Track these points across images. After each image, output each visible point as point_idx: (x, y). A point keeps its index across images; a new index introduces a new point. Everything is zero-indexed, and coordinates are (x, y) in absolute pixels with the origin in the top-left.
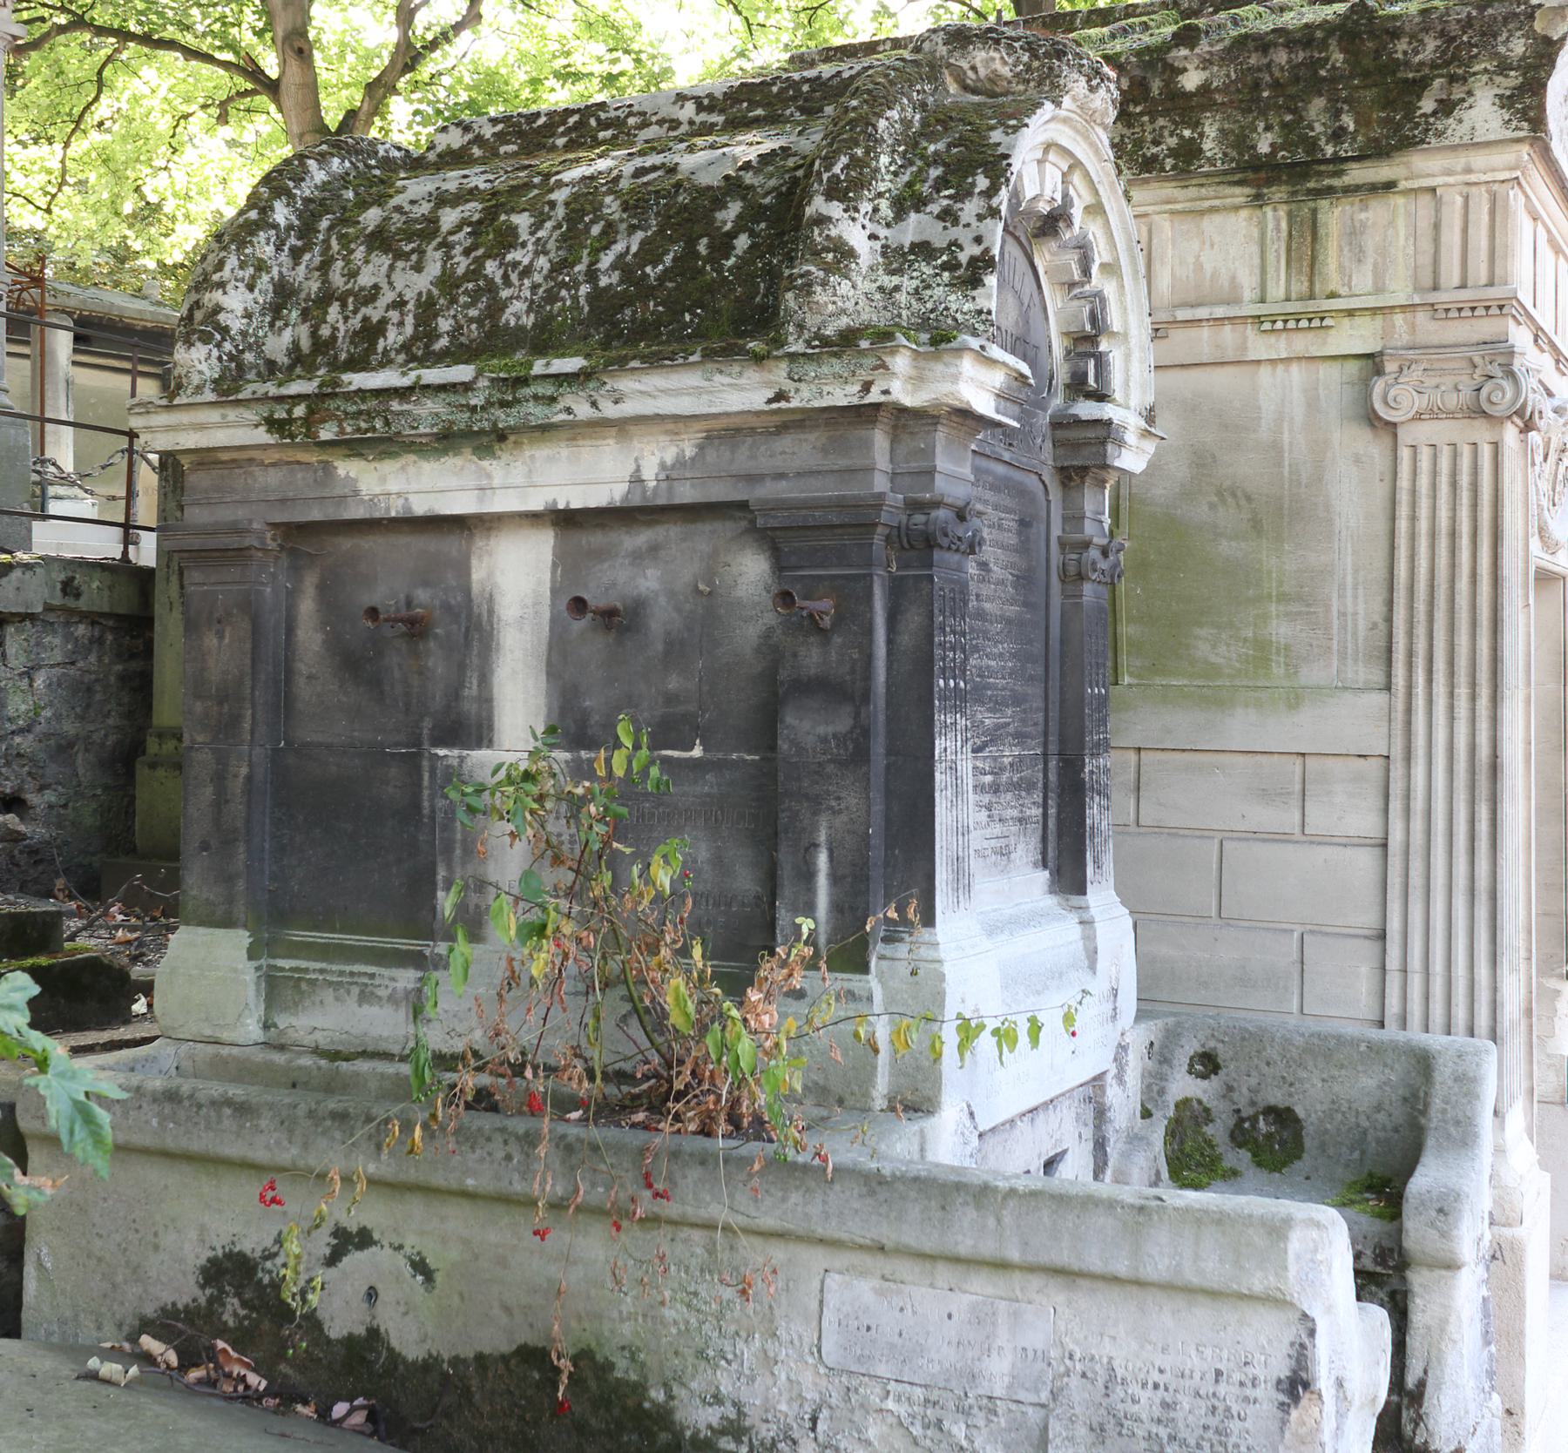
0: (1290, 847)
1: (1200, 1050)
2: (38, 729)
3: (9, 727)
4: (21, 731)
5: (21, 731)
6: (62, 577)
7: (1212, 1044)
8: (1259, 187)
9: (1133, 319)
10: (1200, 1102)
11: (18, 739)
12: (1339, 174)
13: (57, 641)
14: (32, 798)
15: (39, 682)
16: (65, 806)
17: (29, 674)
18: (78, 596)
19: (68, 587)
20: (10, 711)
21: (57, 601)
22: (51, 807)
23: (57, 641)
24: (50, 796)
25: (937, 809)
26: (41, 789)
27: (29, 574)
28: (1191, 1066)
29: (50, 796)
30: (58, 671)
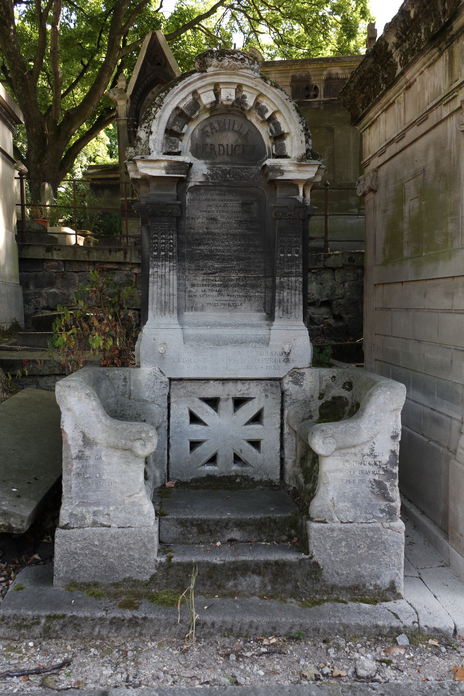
0: (450, 315)
1: (348, 381)
2: (346, 298)
3: (337, 297)
4: (340, 298)
5: (340, 298)
6: (349, 257)
7: (352, 379)
8: (438, 46)
9: (291, 127)
10: (346, 399)
11: (340, 300)
12: (451, 29)
13: (351, 274)
14: (344, 316)
15: (346, 285)
16: (355, 318)
17: (343, 283)
18: (354, 261)
19: (350, 259)
20: (337, 293)
21: (347, 263)
22: (350, 318)
23: (351, 274)
24: (350, 316)
25: (150, 288)
26: (347, 314)
27: (336, 257)
28: (344, 385)
29: (350, 316)
30: (352, 282)
